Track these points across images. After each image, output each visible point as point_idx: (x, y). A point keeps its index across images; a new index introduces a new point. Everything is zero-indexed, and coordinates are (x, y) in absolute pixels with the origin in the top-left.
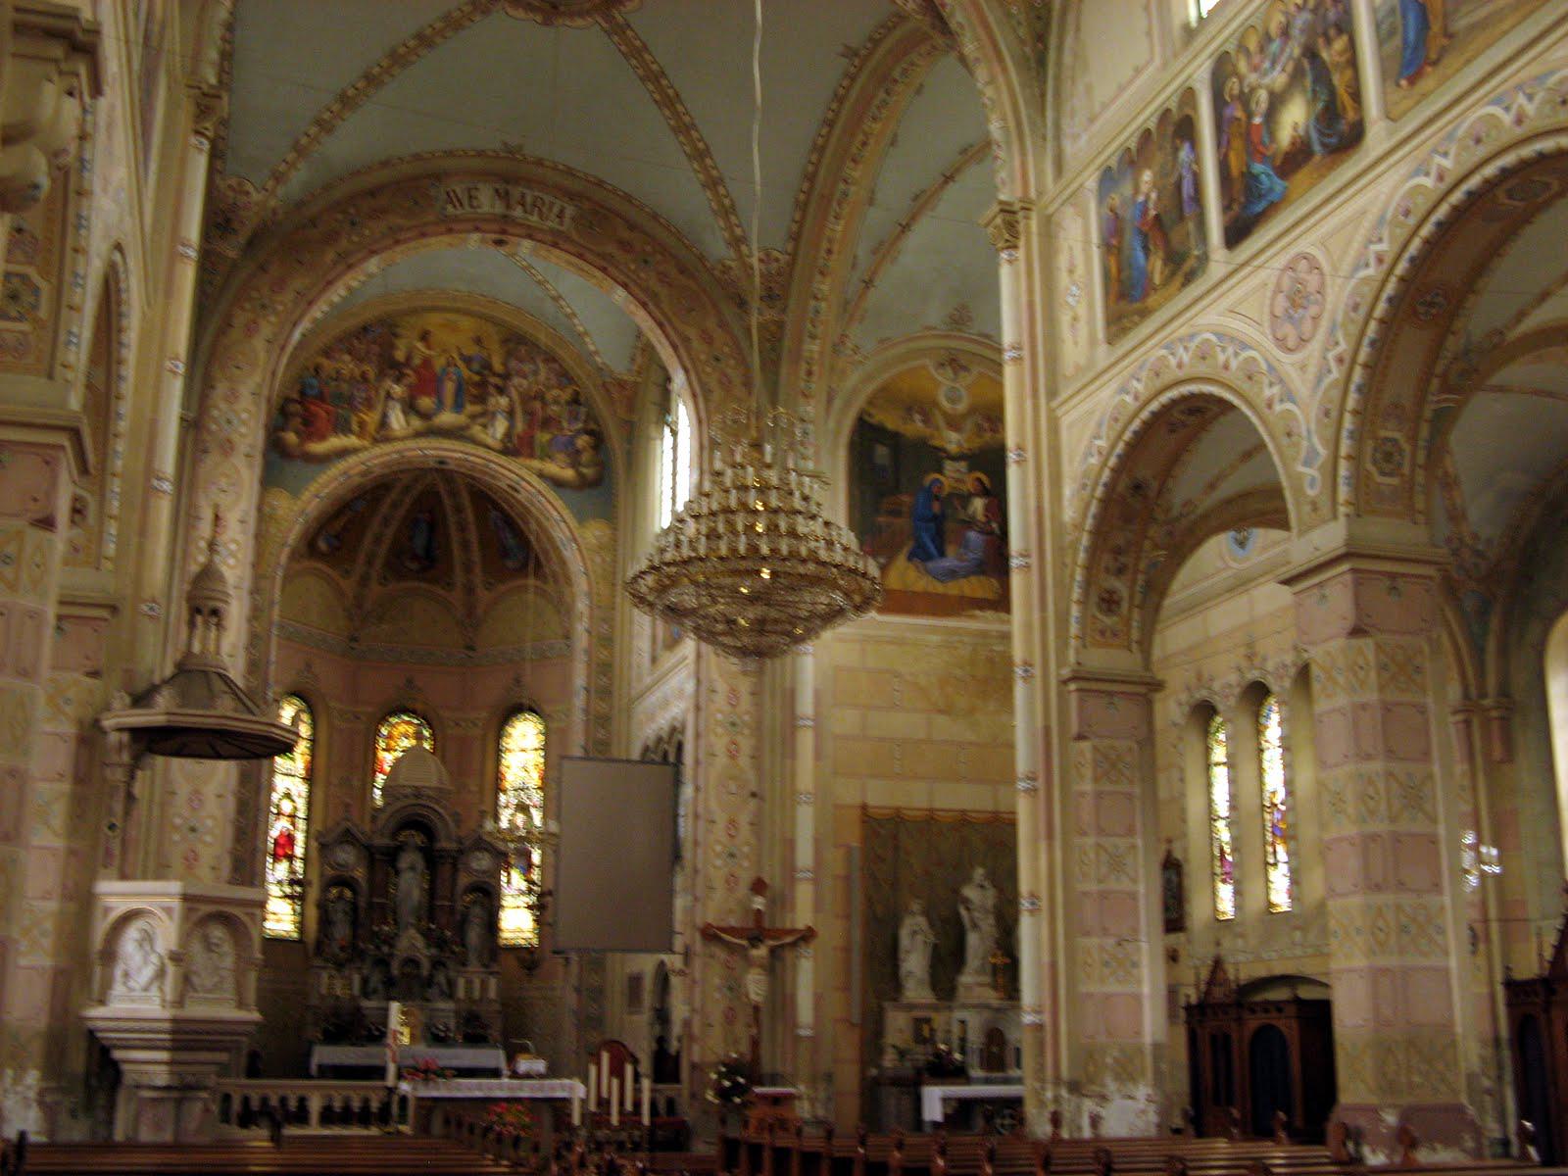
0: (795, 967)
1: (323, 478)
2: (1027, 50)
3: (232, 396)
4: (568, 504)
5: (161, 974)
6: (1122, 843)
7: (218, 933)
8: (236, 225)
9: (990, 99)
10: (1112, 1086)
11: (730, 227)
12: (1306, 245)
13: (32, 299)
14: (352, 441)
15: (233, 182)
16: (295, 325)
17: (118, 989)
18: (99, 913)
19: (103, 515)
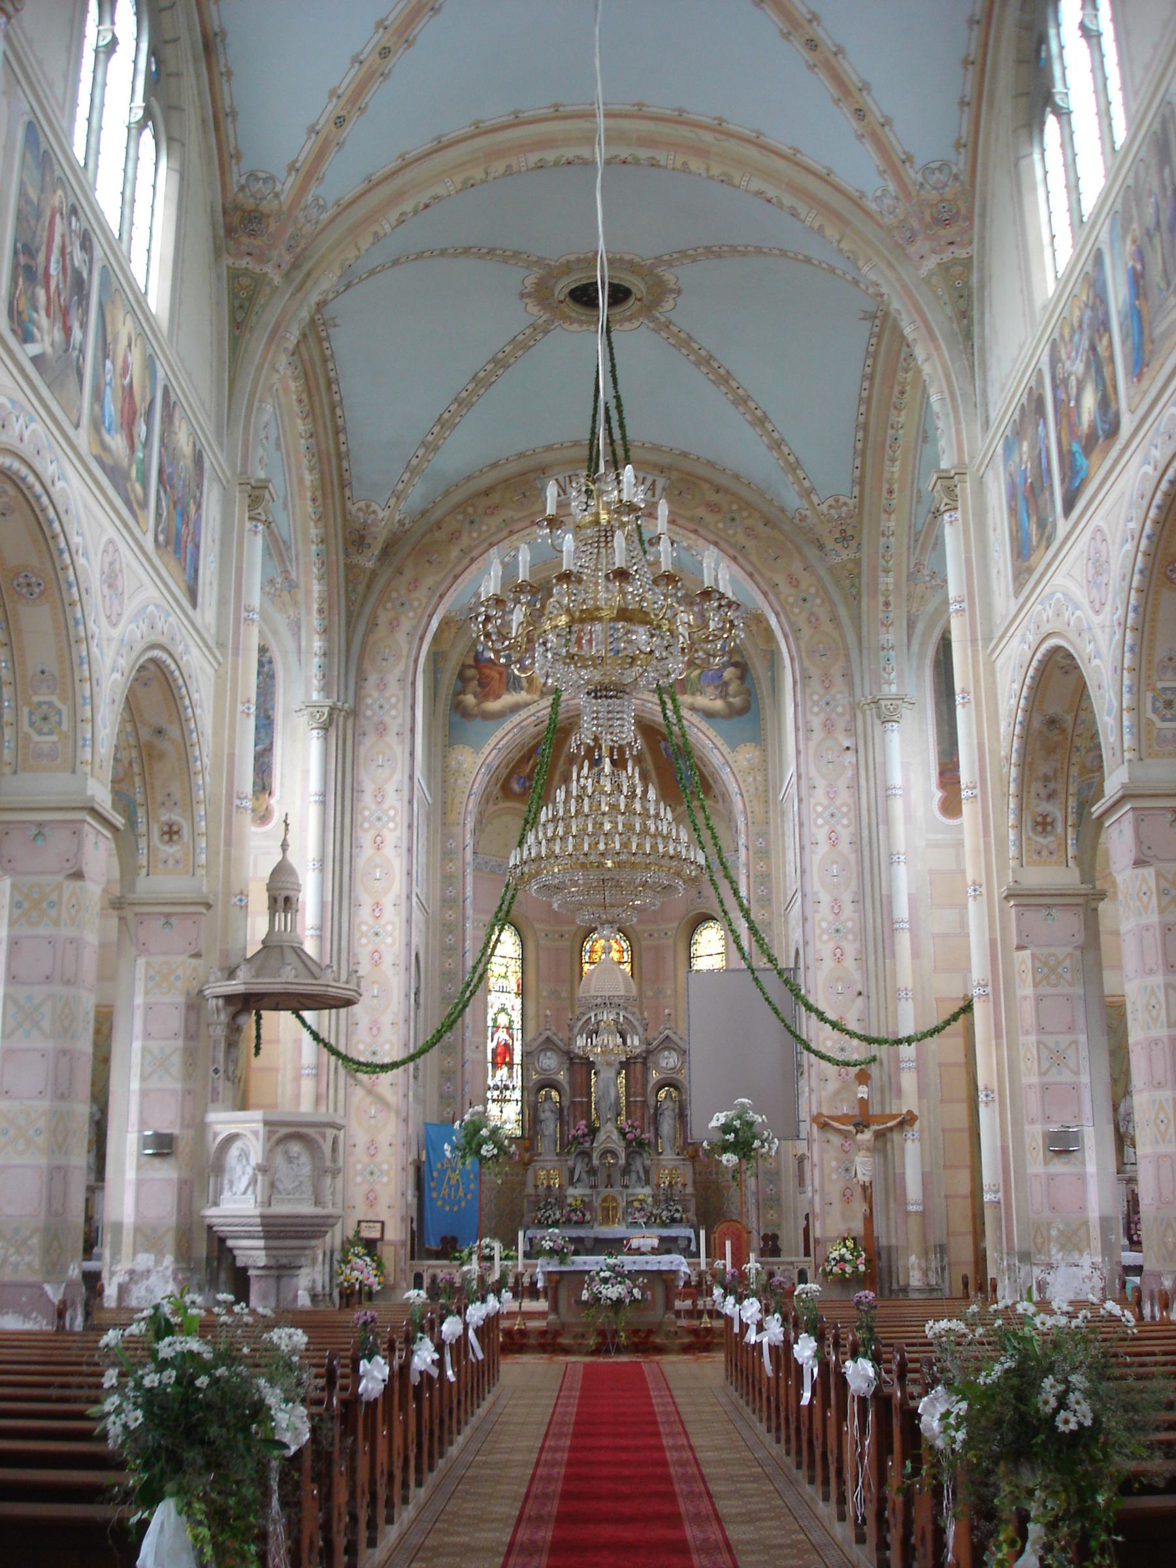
0: (903, 1150)
1: (500, 733)
2: (955, 325)
3: (382, 686)
4: (719, 732)
5: (253, 1181)
6: (1064, 1040)
7: (295, 1148)
8: (369, 540)
9: (928, 375)
10: (1056, 1256)
11: (798, 481)
12: (1098, 521)
13: (57, 718)
14: (523, 696)
15: (362, 504)
16: (430, 617)
17: (226, 1195)
18: (210, 1137)
19: (194, 834)
